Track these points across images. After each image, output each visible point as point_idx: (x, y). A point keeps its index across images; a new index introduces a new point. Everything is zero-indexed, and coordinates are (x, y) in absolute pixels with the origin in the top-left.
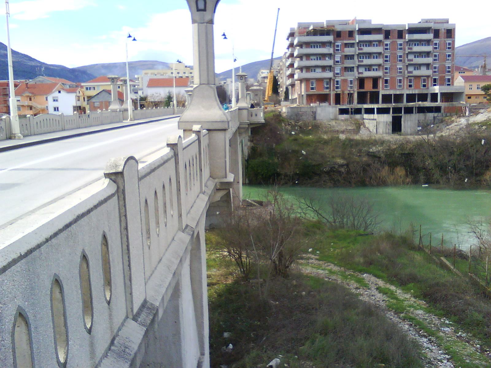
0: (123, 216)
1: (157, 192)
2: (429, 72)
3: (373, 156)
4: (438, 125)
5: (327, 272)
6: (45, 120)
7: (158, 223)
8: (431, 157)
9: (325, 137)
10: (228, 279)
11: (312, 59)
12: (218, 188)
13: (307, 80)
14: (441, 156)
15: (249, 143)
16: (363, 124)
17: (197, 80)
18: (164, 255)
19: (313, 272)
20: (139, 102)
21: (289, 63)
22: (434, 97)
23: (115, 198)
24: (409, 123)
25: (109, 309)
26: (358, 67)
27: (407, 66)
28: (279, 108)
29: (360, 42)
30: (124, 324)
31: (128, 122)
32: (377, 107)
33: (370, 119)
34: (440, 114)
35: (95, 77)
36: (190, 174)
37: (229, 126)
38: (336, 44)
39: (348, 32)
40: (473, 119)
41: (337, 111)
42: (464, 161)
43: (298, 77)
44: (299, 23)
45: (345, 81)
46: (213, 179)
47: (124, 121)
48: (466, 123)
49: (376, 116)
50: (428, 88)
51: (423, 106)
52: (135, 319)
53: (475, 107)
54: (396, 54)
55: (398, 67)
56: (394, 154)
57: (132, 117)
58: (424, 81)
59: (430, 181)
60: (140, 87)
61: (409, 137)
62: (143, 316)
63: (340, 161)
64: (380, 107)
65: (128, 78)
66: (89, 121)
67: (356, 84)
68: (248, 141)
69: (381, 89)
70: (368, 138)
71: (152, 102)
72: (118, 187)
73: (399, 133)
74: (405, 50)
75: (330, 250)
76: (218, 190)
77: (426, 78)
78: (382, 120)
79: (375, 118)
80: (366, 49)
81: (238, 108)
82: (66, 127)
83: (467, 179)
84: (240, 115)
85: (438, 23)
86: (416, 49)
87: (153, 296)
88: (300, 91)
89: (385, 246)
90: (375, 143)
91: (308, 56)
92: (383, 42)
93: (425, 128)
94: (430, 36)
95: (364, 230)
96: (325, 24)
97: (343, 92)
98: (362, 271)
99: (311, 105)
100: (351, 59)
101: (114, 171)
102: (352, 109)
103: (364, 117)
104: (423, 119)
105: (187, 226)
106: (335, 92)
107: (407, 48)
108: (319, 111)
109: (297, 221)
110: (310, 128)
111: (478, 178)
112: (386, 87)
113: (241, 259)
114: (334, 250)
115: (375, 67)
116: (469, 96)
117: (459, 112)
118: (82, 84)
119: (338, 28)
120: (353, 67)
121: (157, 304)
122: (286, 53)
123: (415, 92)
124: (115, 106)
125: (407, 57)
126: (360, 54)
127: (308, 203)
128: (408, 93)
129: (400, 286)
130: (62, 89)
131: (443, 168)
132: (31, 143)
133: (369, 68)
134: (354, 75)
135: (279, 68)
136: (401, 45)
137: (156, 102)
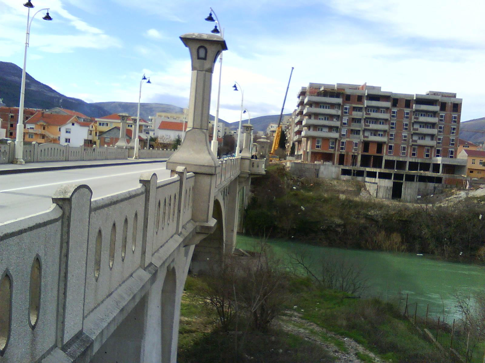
0: (65, 242)
1: (116, 225)
2: (433, 143)
3: (371, 219)
4: (437, 195)
5: (307, 332)
6: (56, 150)
7: (112, 256)
8: (428, 226)
9: (326, 195)
10: (207, 328)
11: (320, 119)
12: (198, 232)
13: (313, 138)
14: (438, 226)
15: (250, 194)
16: (364, 186)
17: (190, 125)
18: (116, 289)
19: (294, 330)
20: (148, 142)
21: (298, 120)
22: (436, 167)
23: (59, 223)
24: (409, 191)
25: (33, 334)
26: (365, 130)
27: (412, 135)
28: (283, 162)
29: (368, 107)
30: (50, 352)
31: (133, 160)
32: (379, 171)
33: (371, 183)
34: (440, 185)
35: (110, 114)
36: (165, 213)
37: (215, 171)
38: (345, 107)
39: (357, 97)
40: (472, 194)
41: (339, 171)
42: (460, 234)
43: (305, 134)
44: (310, 83)
45: (350, 143)
46: (195, 222)
47: (128, 159)
48: (465, 196)
49: (377, 180)
50: (431, 158)
51: (424, 175)
52: (64, 349)
53: (476, 182)
54: (402, 122)
55: (403, 134)
56: (391, 220)
57: (137, 155)
58: (428, 151)
59: (425, 251)
60: (152, 128)
61: (408, 204)
62: (74, 347)
63: (338, 221)
64: (382, 171)
65: (138, 118)
66: (93, 154)
67: (361, 146)
68: (250, 191)
69: (384, 154)
70: (368, 201)
71: (161, 143)
72: (64, 212)
73: (398, 199)
74: (411, 119)
75: (315, 309)
76: (198, 233)
77: (430, 148)
78: (383, 185)
79: (376, 182)
80: (374, 115)
81: (240, 157)
82: (70, 158)
83: (461, 253)
84: (241, 164)
85: (445, 96)
86: (422, 119)
87: (91, 329)
88: (306, 148)
89: (370, 311)
90: (374, 206)
91: (316, 115)
92: (391, 109)
93: (425, 197)
94: (437, 108)
95: (353, 293)
96: (336, 86)
97: (347, 153)
98: (343, 335)
99: (315, 162)
100: (358, 122)
101: (62, 197)
102: (354, 170)
103: (366, 180)
104: (424, 188)
105: (151, 264)
106: (340, 153)
107: (413, 117)
108: (322, 169)
109: (285, 276)
110: (312, 185)
111: (472, 253)
112: (390, 152)
113: (223, 309)
114: (319, 310)
115: (381, 133)
116: (472, 170)
117: (460, 185)
118: (96, 119)
119: (348, 92)
120: (359, 131)
121: (94, 337)
122: (296, 110)
123: (418, 160)
124: (122, 143)
125: (413, 126)
126: (366, 118)
127: (300, 259)
128: (411, 160)
129: (380, 354)
130: (76, 122)
131: (439, 239)
132: (30, 169)
133: (375, 132)
134: (359, 138)
135: (288, 124)
136: (408, 114)
137: (165, 144)
